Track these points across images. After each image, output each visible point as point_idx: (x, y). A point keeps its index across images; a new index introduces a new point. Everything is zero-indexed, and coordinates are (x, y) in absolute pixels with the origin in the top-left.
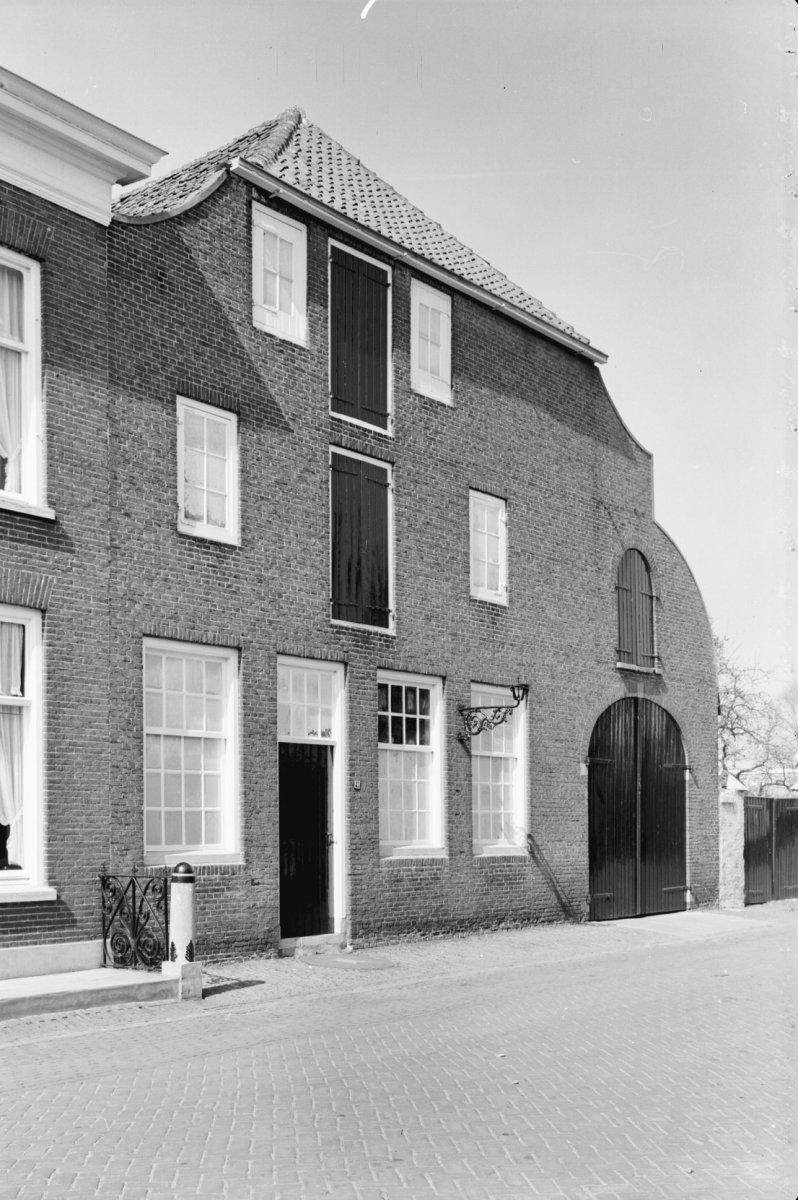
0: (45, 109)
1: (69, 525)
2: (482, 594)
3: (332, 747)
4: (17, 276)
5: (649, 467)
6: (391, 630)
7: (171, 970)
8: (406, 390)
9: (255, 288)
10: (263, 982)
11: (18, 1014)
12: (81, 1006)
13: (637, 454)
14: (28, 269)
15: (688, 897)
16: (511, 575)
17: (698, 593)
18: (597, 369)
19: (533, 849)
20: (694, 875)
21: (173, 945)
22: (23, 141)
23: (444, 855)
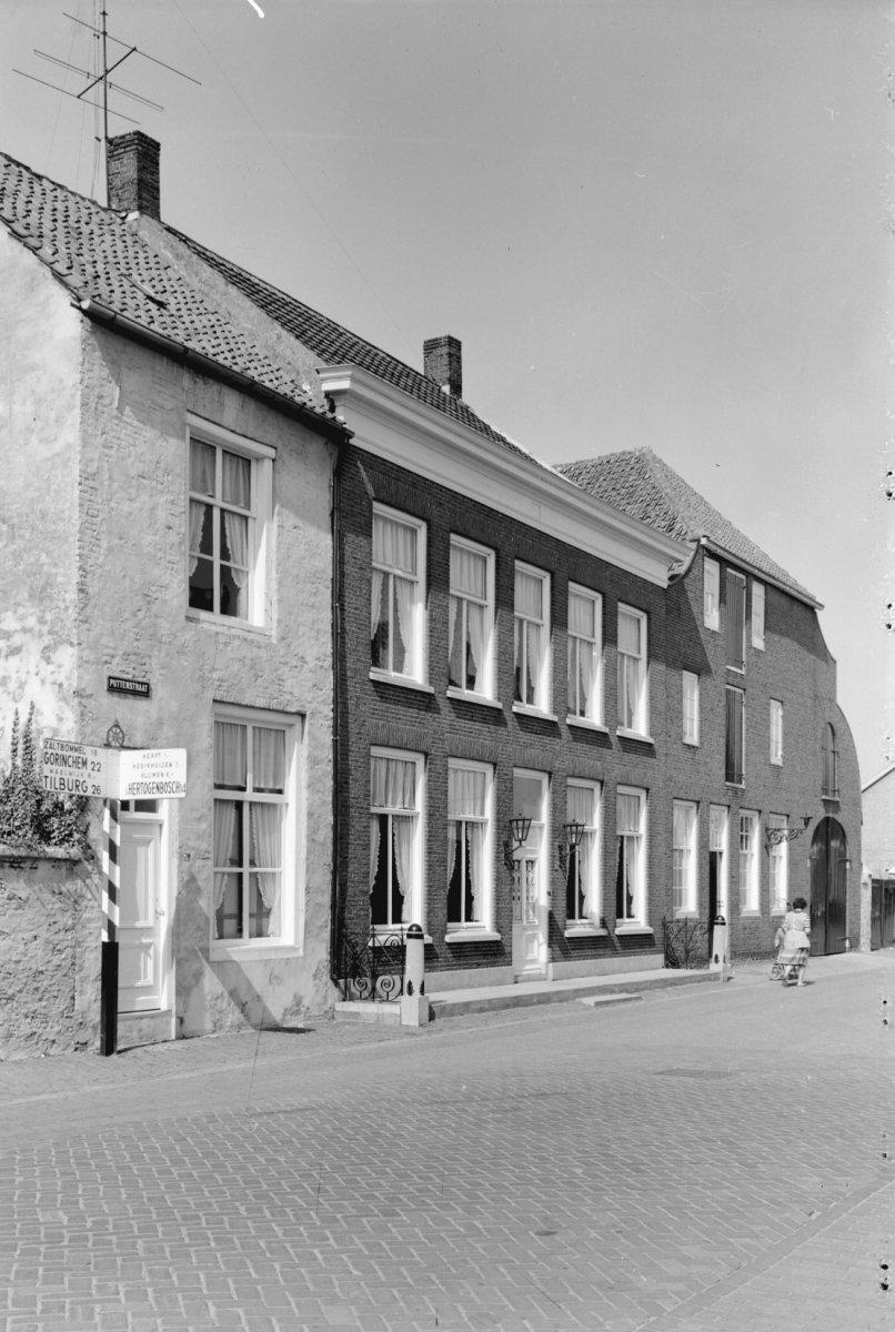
1: (660, 751)
2: (687, 740)
3: (721, 853)
4: (414, 532)
5: (835, 668)
6: (743, 786)
7: (714, 968)
8: (750, 647)
9: (411, 470)
13: (831, 661)
15: (847, 944)
16: (784, 748)
17: (854, 747)
18: (815, 613)
20: (850, 931)
23: (758, 914)
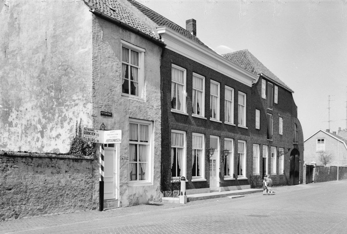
0: (216, 56)
4: (183, 72)
10: (163, 205)
11: (256, 192)
12: (252, 193)
14: (185, 70)
15: (300, 182)
18: (292, 94)
19: (284, 173)
21: (182, 192)
22: (228, 69)
